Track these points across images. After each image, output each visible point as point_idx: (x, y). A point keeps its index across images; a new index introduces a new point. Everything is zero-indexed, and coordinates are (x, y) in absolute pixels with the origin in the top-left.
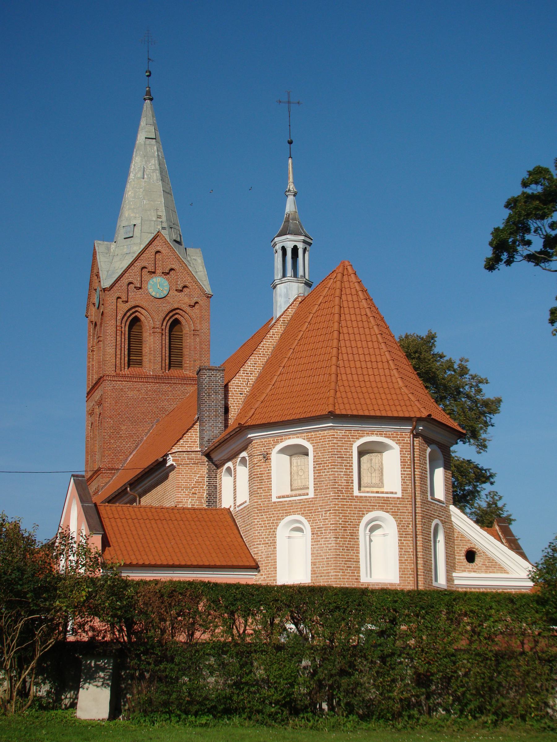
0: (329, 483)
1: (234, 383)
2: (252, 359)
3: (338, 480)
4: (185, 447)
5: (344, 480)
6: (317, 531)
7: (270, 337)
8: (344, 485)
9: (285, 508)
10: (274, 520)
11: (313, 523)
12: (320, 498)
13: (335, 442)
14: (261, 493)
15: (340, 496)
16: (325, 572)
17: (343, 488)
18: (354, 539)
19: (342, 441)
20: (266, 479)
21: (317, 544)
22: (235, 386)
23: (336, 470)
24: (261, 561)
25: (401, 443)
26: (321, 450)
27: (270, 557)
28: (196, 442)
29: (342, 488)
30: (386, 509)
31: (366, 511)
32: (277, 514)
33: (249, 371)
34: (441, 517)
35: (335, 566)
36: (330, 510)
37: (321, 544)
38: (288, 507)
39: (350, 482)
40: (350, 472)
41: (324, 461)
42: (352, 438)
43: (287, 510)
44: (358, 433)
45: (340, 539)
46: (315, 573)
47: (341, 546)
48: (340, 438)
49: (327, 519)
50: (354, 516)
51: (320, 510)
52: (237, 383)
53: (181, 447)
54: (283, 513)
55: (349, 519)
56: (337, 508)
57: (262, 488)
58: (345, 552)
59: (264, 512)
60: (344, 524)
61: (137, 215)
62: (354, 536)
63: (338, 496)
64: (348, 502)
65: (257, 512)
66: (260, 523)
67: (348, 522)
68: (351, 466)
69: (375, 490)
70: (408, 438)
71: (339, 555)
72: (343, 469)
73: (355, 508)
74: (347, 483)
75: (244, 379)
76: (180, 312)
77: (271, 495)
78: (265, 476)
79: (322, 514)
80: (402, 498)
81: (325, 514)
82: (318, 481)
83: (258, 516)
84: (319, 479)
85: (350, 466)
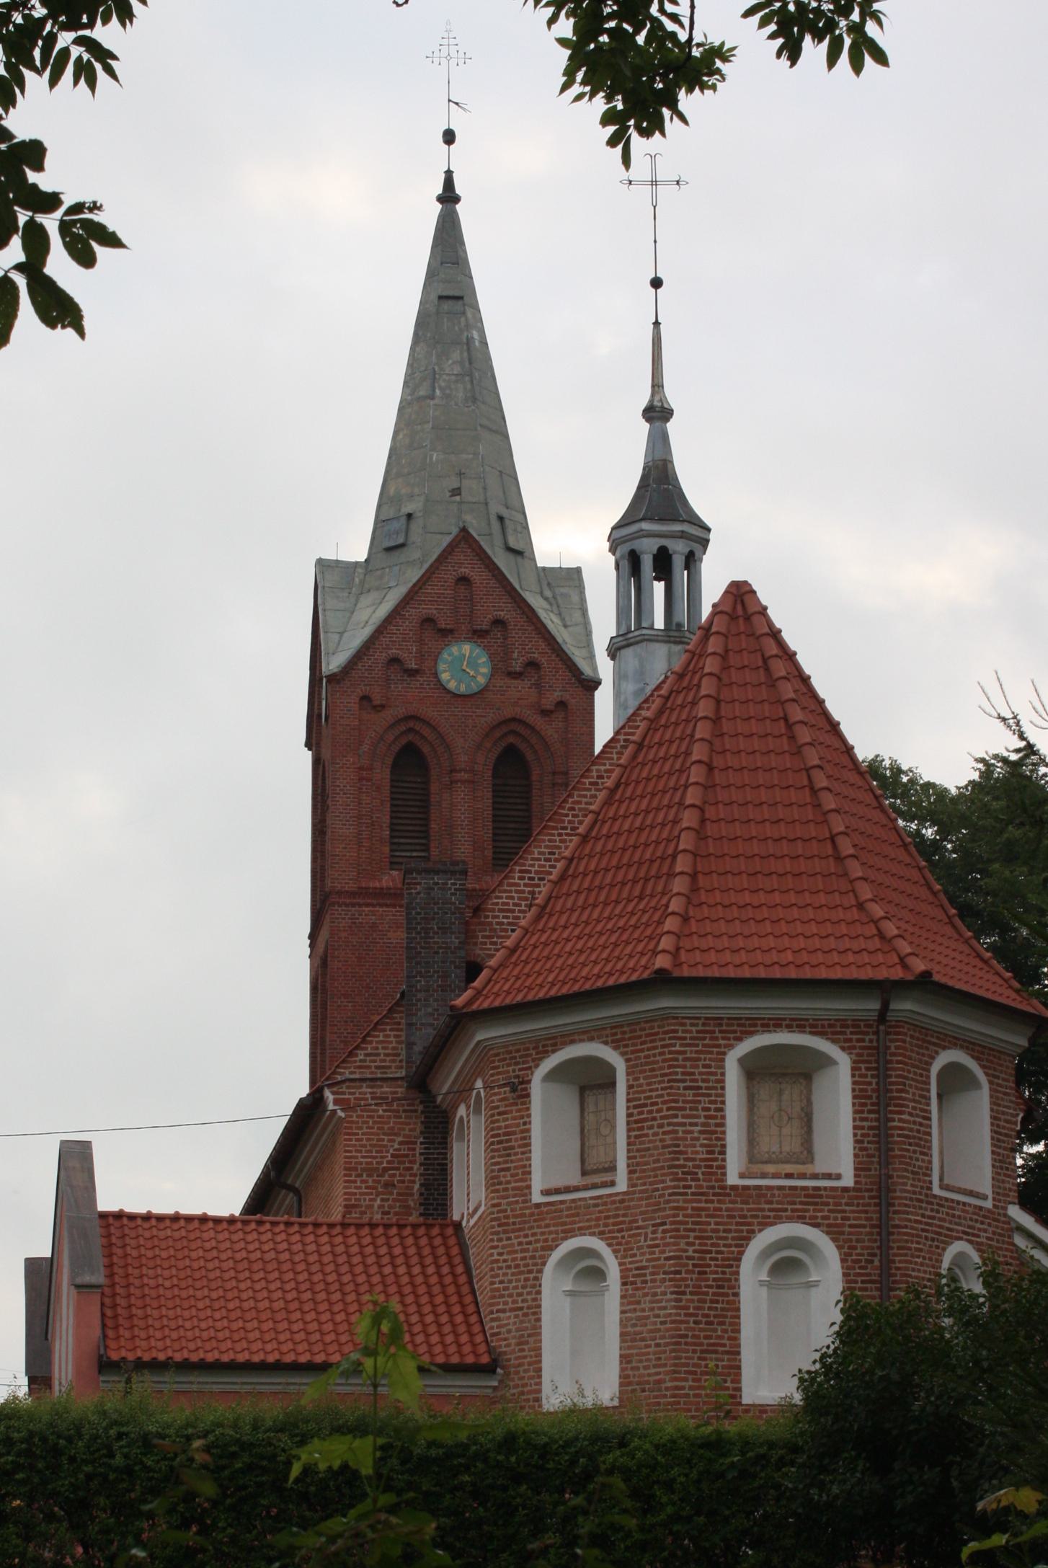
0: (663, 1154)
1: (497, 904)
2: (544, 841)
3: (685, 1146)
4: (369, 1067)
5: (702, 1145)
6: (634, 1276)
7: (591, 784)
8: (702, 1160)
9: (561, 1218)
10: (535, 1250)
11: (625, 1257)
12: (641, 1192)
13: (677, 1048)
14: (508, 1182)
15: (690, 1187)
16: (651, 1379)
17: (699, 1167)
18: (727, 1295)
19: (697, 1045)
20: (520, 1146)
21: (635, 1310)
22: (500, 911)
23: (680, 1120)
24: (505, 1353)
25: (854, 1048)
26: (645, 1071)
27: (527, 1343)
28: (398, 1055)
29: (695, 1167)
30: (812, 1218)
31: (759, 1224)
32: (543, 1233)
33: (536, 872)
34: (978, 1236)
35: (675, 1365)
36: (664, 1224)
37: (643, 1310)
38: (567, 1216)
39: (717, 1150)
40: (717, 1125)
41: (650, 1097)
42: (723, 1038)
43: (564, 1224)
44: (739, 1025)
45: (689, 1297)
46: (630, 1384)
47: (691, 1315)
48: (691, 1038)
49: (657, 1246)
50: (726, 1238)
51: (640, 1223)
52: (504, 904)
53: (360, 1067)
54: (557, 1232)
55: (712, 1245)
56: (681, 1218)
57: (508, 1169)
58: (701, 1330)
59: (513, 1231)
60: (700, 1259)
61: (416, 490)
62: (727, 1288)
63: (685, 1187)
64: (712, 1202)
65: (497, 1229)
66: (505, 1257)
67: (710, 1252)
68: (722, 1110)
69: (789, 1168)
70: (874, 1033)
71: (686, 1336)
72: (698, 1117)
73: (729, 1217)
74: (708, 1152)
75: (523, 892)
76: (520, 729)
77: (529, 1187)
78: (516, 1140)
79: (646, 1234)
80: (854, 1189)
81: (654, 1232)
82: (638, 1150)
83: (500, 1240)
84: (641, 1143)
85: (717, 1110)
